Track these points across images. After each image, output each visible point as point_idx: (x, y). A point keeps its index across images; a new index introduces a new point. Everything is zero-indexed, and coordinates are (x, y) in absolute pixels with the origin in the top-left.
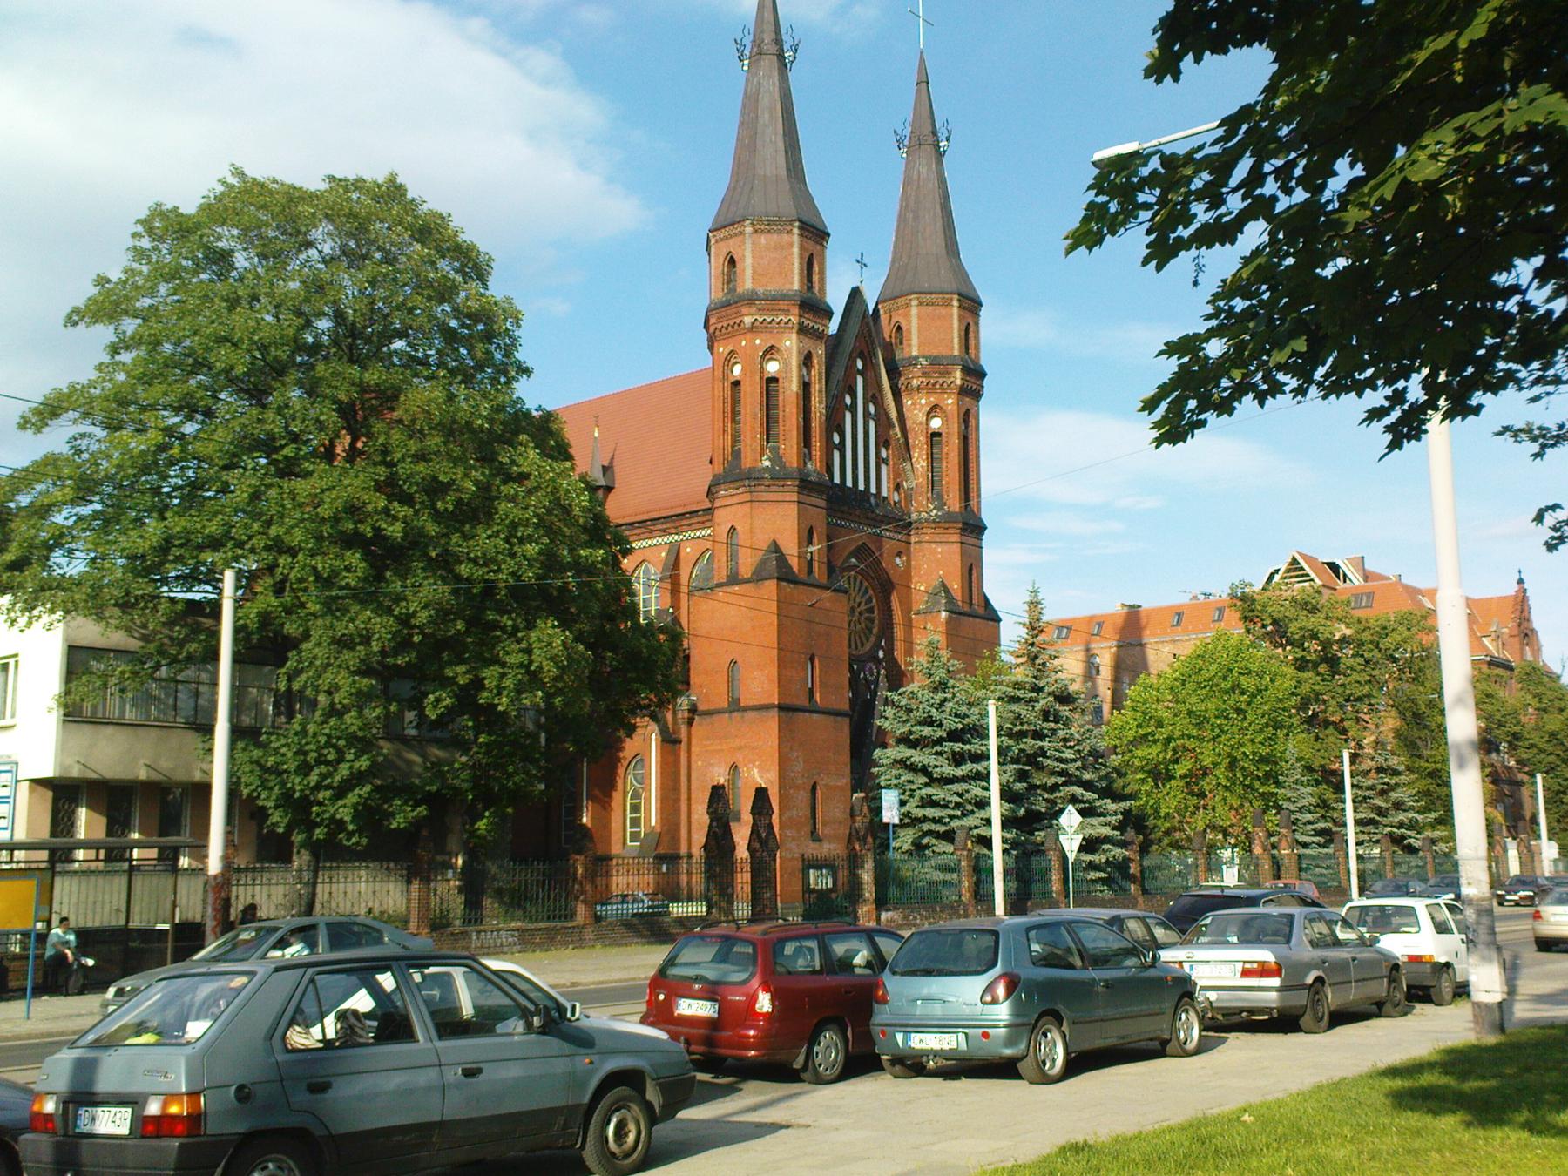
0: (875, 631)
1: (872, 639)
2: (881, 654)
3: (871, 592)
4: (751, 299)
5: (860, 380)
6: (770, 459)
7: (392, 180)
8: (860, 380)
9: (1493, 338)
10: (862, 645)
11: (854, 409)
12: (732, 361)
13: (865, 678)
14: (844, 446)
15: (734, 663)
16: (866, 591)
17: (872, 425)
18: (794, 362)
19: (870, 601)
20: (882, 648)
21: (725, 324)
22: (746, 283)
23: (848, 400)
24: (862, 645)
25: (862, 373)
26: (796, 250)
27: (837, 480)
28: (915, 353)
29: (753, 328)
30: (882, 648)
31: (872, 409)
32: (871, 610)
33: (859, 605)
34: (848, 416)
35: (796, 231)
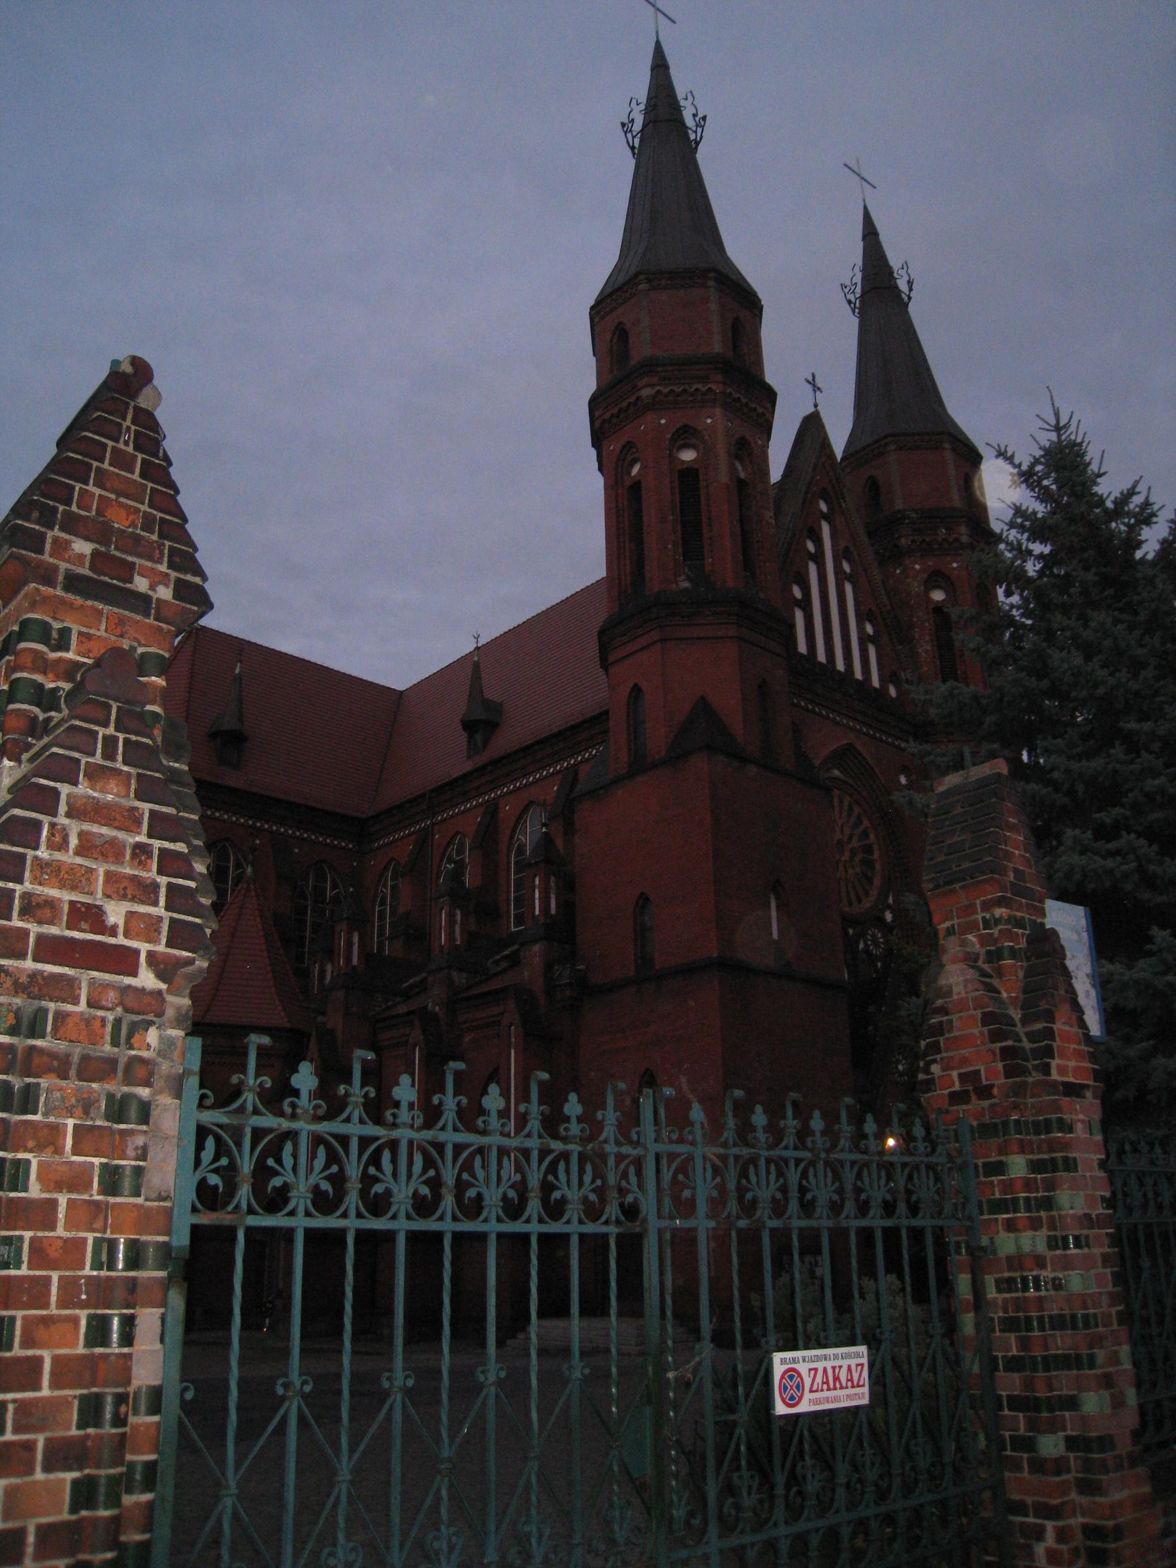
0: (877, 881)
1: (874, 893)
2: (889, 917)
3: (866, 822)
4: (649, 367)
5: (825, 528)
6: (688, 579)
7: (501, 704)
8: (825, 528)
9: (1014, 853)
10: (860, 901)
11: (818, 558)
12: (629, 458)
13: (867, 951)
14: (823, 553)
15: (644, 900)
16: (859, 821)
17: (848, 588)
18: (722, 448)
19: (865, 835)
20: (889, 907)
21: (615, 411)
22: (641, 349)
23: (797, 592)
24: (860, 901)
25: (825, 517)
26: (713, 306)
27: (802, 648)
28: (899, 505)
29: (655, 405)
30: (889, 907)
31: (846, 567)
32: (868, 850)
33: (850, 838)
34: (799, 616)
35: (711, 283)
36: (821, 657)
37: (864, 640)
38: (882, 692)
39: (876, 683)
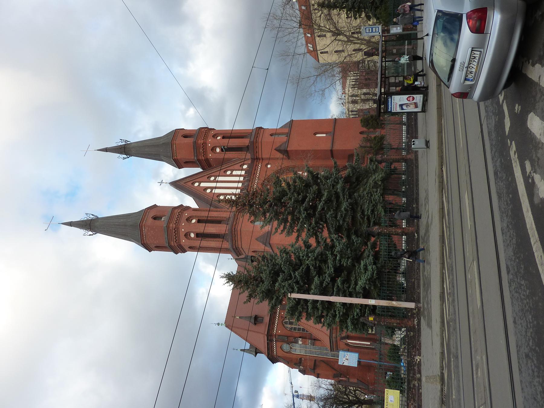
11: (212, 188)
36: (240, 185)
37: (231, 175)
38: (247, 171)
39: (243, 173)
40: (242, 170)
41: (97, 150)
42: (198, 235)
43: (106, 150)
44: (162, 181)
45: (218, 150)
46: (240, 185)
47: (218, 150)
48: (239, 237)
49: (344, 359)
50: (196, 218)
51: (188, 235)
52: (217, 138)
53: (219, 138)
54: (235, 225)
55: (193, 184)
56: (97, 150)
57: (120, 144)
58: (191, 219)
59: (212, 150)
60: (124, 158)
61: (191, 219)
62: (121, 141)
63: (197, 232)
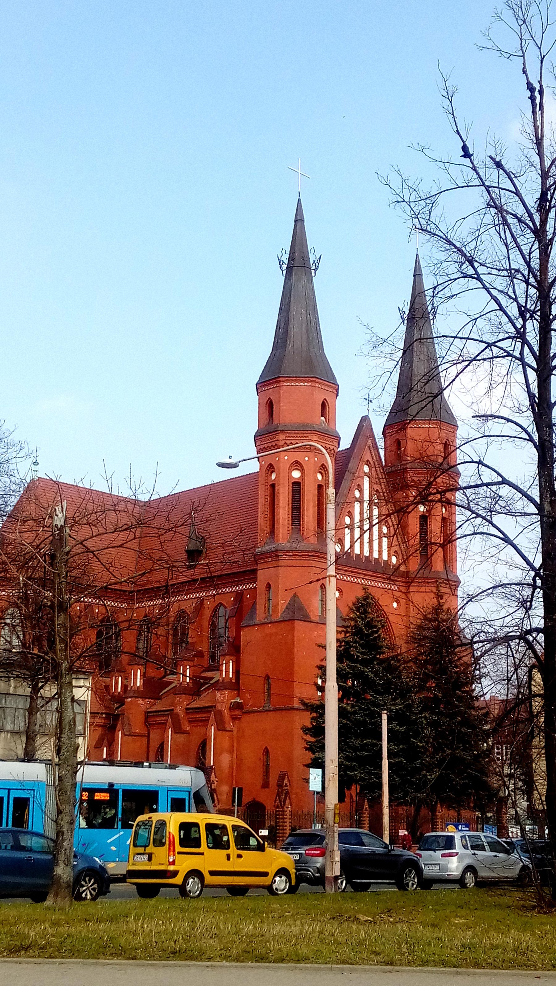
11: (361, 501)
36: (376, 555)
39: (385, 557)
40: (389, 556)
41: (299, 200)
42: (297, 486)
43: (299, 220)
44: (366, 400)
45: (296, 474)
46: (357, 551)
47: (296, 474)
48: (299, 563)
49: (315, 775)
50: (324, 482)
51: (296, 466)
52: (320, 472)
53: (319, 477)
54: (318, 556)
55: (368, 463)
56: (299, 200)
57: (312, 258)
58: (323, 471)
59: (297, 462)
60: (402, 312)
61: (323, 471)
62: (318, 257)
63: (304, 485)
